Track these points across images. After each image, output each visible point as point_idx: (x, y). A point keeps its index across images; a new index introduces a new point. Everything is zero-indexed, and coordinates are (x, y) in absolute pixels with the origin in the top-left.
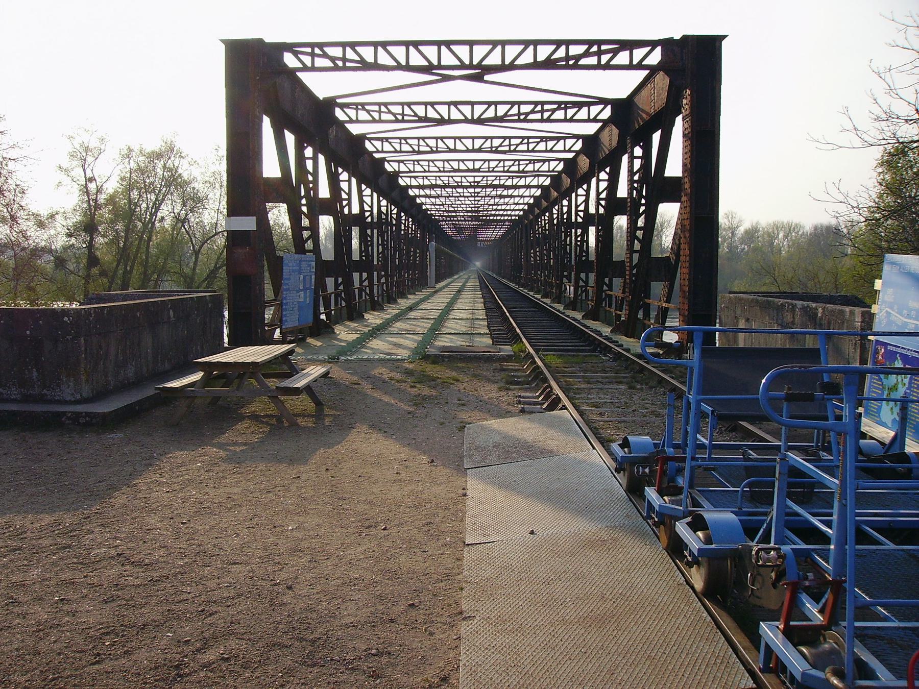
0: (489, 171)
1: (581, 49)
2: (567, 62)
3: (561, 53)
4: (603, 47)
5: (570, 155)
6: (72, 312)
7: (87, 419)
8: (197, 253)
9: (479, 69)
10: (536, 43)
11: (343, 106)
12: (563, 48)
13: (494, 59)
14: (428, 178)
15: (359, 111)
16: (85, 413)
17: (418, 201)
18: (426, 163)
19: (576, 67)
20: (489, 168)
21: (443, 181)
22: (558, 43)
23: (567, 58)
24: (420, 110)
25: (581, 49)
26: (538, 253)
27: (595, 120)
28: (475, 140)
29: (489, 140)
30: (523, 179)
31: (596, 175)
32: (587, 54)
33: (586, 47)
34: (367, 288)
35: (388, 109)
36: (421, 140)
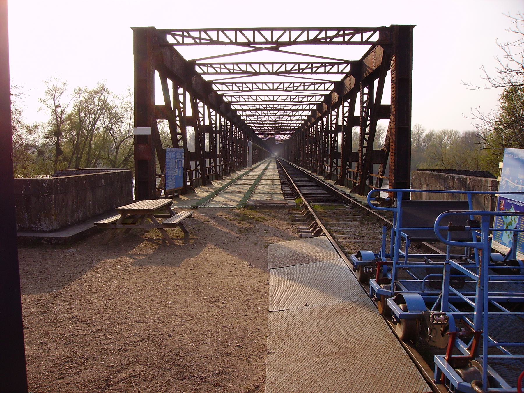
2: (326, 40)
3: (322, 35)
4: (346, 32)
8: (117, 148)
10: (308, 29)
11: (200, 65)
12: (324, 32)
13: (285, 38)
18: (247, 97)
19: (331, 43)
20: (282, 100)
21: (256, 107)
22: (321, 30)
23: (326, 37)
26: (309, 148)
27: (342, 73)
29: (282, 84)
30: (301, 106)
31: (342, 103)
32: (337, 36)
34: (214, 167)
36: (244, 84)
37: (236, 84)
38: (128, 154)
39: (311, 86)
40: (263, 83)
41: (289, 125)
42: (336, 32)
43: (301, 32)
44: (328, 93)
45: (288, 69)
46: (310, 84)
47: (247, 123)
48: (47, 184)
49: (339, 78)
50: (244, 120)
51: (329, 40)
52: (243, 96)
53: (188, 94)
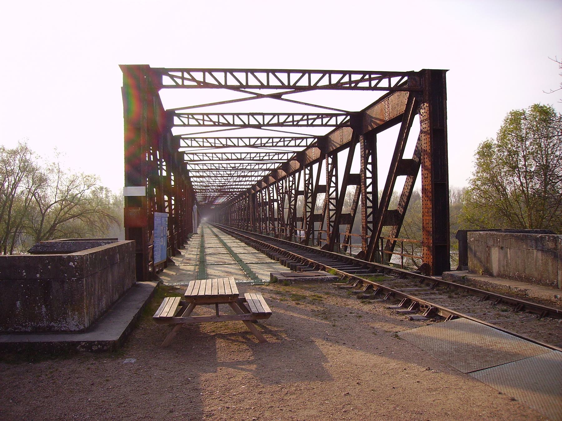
0: (250, 160)
1: (358, 77)
2: (350, 85)
3: (346, 79)
4: (372, 76)
5: (301, 149)
6: (77, 258)
7: (99, 346)
9: (293, 89)
10: (330, 72)
11: (179, 115)
12: (347, 76)
13: (304, 82)
14: (206, 165)
15: (190, 119)
16: (98, 341)
19: (356, 88)
20: (250, 157)
21: (215, 167)
22: (344, 73)
23: (350, 82)
25: (358, 77)
28: (251, 139)
29: (260, 139)
30: (257, 172)
32: (362, 80)
33: (362, 75)
38: (55, 222)
39: (265, 142)
41: (239, 187)
42: (361, 76)
43: (321, 75)
46: (291, 139)
48: (76, 263)
51: (354, 84)
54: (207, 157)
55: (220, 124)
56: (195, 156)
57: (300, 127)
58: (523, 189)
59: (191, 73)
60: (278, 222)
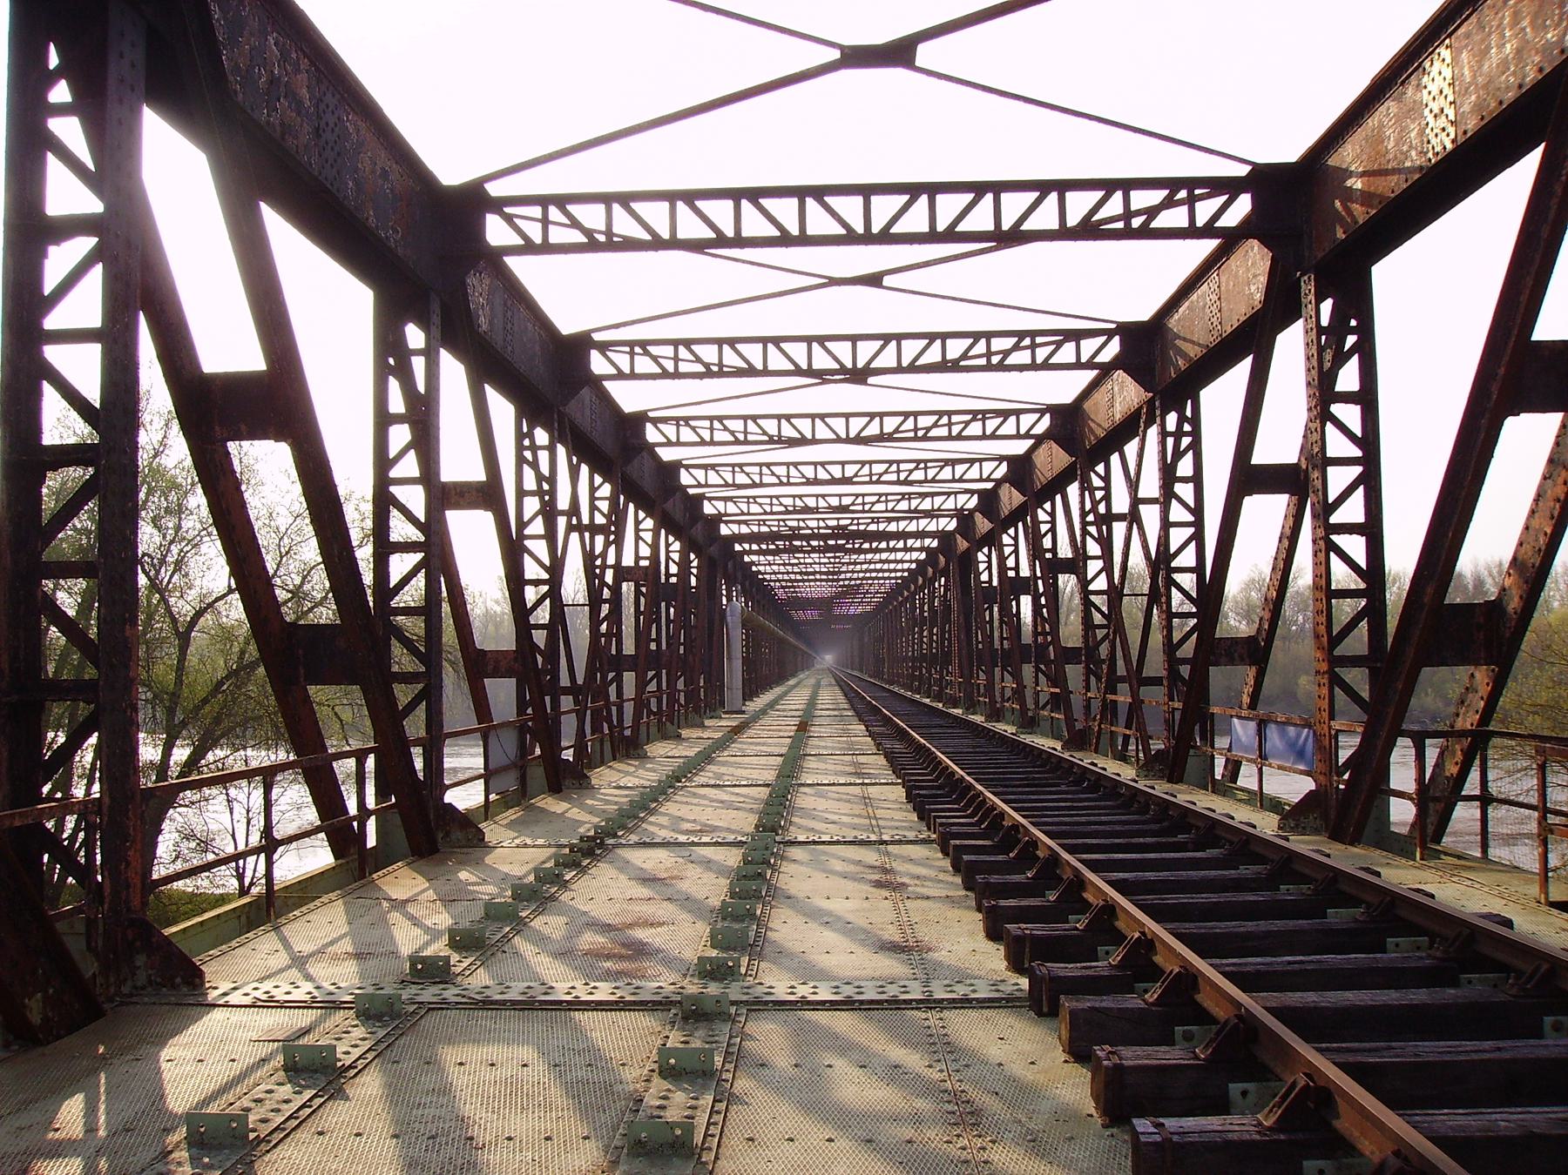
8: (184, 638)
10: (1063, 187)
11: (604, 347)
17: (708, 509)
18: (757, 469)
24: (771, 426)
26: (935, 637)
27: (1027, 436)
30: (915, 521)
31: (1158, 420)
34: (682, 694)
35: (723, 425)
36: (750, 422)
37: (733, 439)
40: (813, 417)
44: (989, 485)
45: (888, 428)
47: (759, 572)
49: (1020, 447)
50: (753, 563)
52: (744, 468)
53: (561, 451)
54: (777, 474)
55: (725, 369)
56: (711, 473)
57: (964, 374)
58: (157, 606)
59: (570, 208)
60: (1087, 667)
